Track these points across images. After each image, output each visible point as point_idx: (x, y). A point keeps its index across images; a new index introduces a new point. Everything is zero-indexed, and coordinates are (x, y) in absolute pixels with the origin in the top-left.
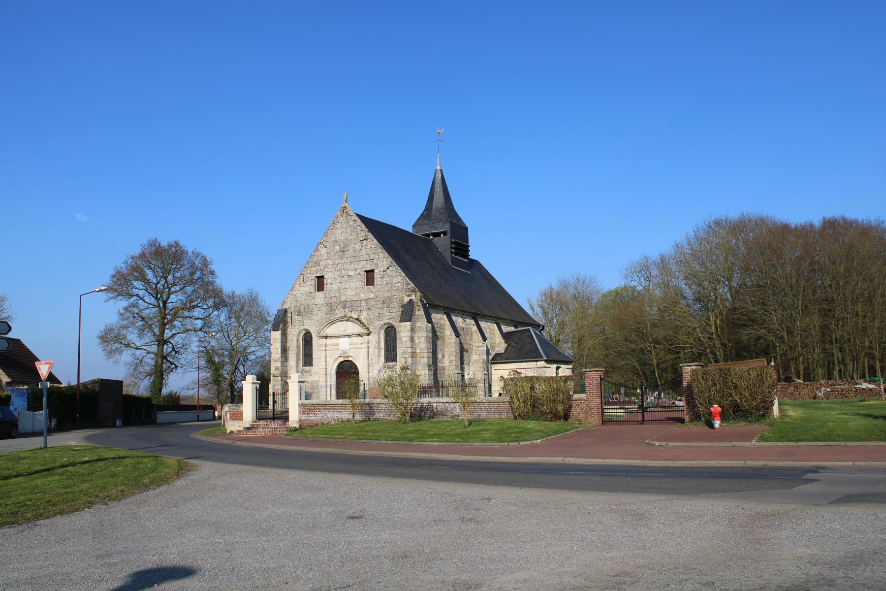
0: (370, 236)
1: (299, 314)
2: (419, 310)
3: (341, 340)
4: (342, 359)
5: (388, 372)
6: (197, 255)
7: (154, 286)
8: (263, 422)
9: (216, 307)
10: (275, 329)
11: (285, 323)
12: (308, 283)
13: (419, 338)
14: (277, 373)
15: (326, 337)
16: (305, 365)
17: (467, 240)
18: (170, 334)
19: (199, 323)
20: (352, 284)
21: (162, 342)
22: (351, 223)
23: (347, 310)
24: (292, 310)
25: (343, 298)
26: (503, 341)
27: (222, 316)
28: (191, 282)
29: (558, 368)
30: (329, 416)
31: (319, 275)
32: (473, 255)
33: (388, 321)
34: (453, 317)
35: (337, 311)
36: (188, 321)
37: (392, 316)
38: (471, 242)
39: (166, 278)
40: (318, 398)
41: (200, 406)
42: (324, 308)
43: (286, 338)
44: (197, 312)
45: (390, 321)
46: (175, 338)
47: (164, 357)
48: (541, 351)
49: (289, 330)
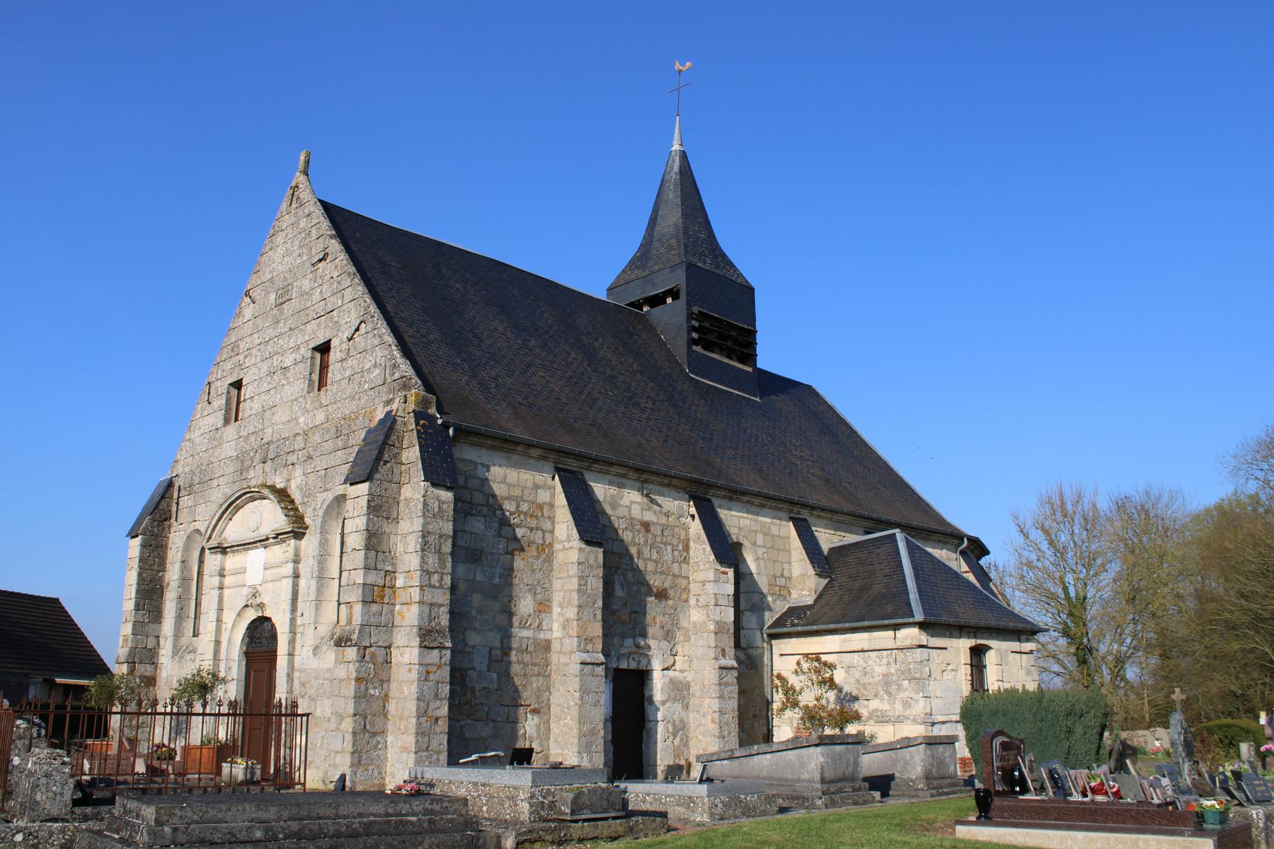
0: (335, 246)
13: (405, 535)
17: (752, 318)
26: (811, 571)
29: (978, 653)
32: (772, 356)
34: (724, 514)
38: (759, 325)
48: (914, 596)
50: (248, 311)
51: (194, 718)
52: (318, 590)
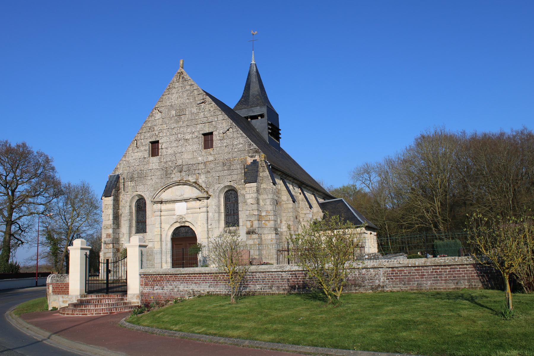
1: (132, 179)
2: (264, 171)
3: (177, 205)
4: (178, 225)
5: (229, 238)
6: (41, 155)
7: (4, 177)
8: (94, 297)
9: (56, 195)
10: (107, 194)
11: (118, 190)
12: (142, 148)
14: (109, 240)
15: (161, 202)
16: (138, 231)
18: (18, 216)
19: (41, 208)
20: (189, 148)
21: (10, 222)
22: (188, 87)
23: (183, 174)
24: (125, 176)
25: (179, 162)
26: (321, 210)
27: (59, 203)
28: (36, 175)
30: (181, 288)
31: (153, 139)
33: (229, 184)
35: (173, 176)
36: (32, 207)
37: (235, 179)
39: (15, 173)
40: (153, 265)
41: (39, 274)
42: (159, 173)
43: (118, 205)
44: (40, 199)
45: (232, 184)
46: (22, 220)
47: (11, 235)
49: (121, 196)
50: (158, 116)
51: (39, 264)
52: (219, 217)
